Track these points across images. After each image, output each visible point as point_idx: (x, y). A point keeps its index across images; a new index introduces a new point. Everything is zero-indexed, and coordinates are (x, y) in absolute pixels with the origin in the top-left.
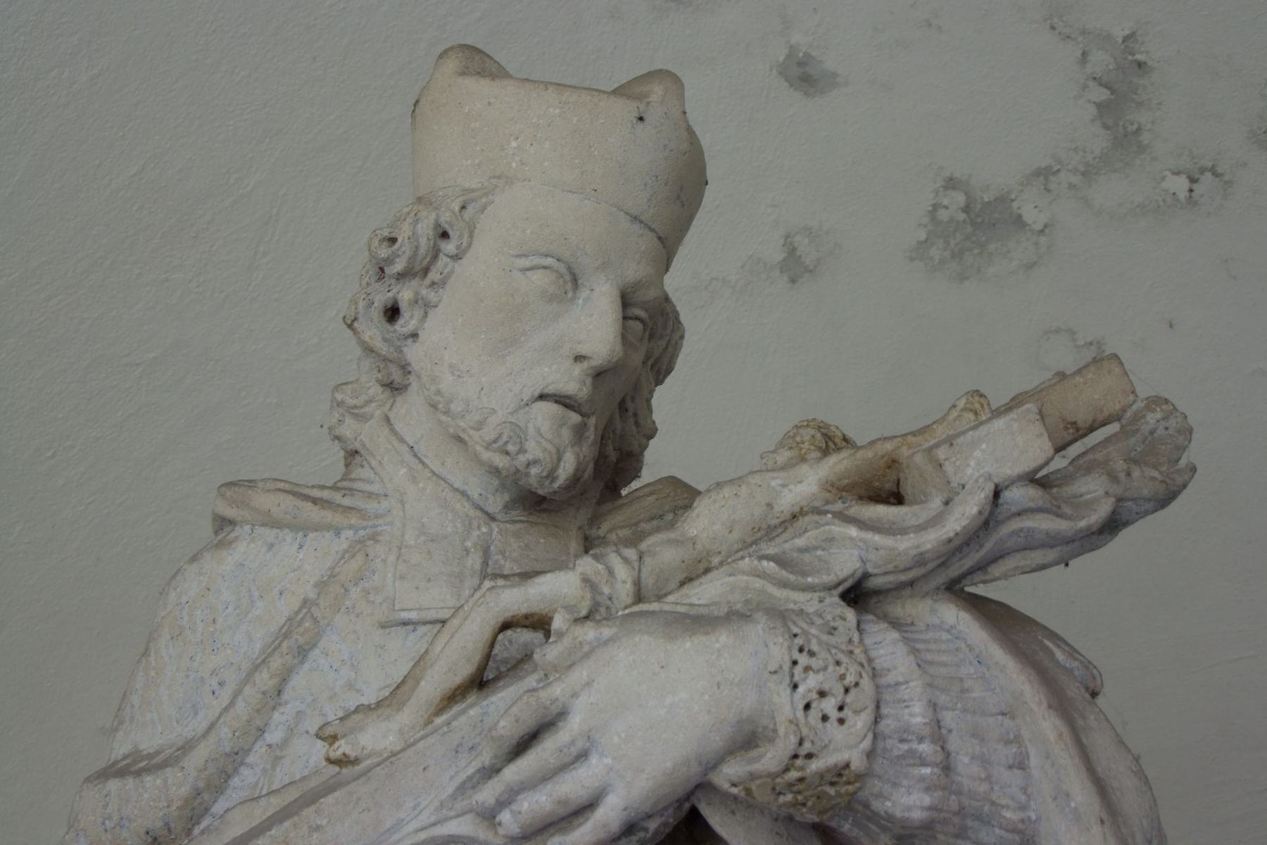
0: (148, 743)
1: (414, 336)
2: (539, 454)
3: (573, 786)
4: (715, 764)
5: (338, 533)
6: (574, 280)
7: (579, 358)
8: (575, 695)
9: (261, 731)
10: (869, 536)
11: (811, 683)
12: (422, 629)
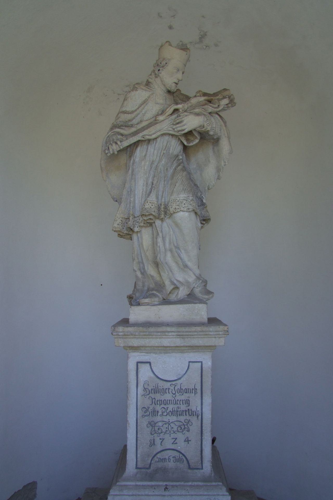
0: (128, 110)
1: (161, 73)
2: (173, 89)
3: (183, 128)
4: (197, 128)
5: (150, 92)
6: (178, 70)
7: (178, 79)
8: (185, 120)
9: (141, 112)
10: (213, 108)
11: (207, 122)
12: (160, 105)
